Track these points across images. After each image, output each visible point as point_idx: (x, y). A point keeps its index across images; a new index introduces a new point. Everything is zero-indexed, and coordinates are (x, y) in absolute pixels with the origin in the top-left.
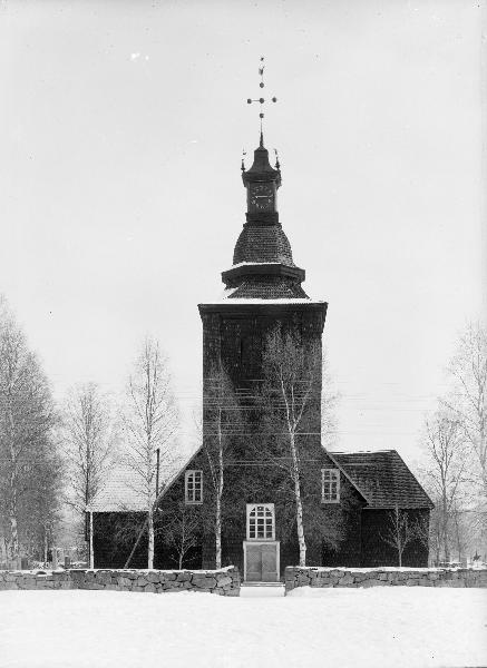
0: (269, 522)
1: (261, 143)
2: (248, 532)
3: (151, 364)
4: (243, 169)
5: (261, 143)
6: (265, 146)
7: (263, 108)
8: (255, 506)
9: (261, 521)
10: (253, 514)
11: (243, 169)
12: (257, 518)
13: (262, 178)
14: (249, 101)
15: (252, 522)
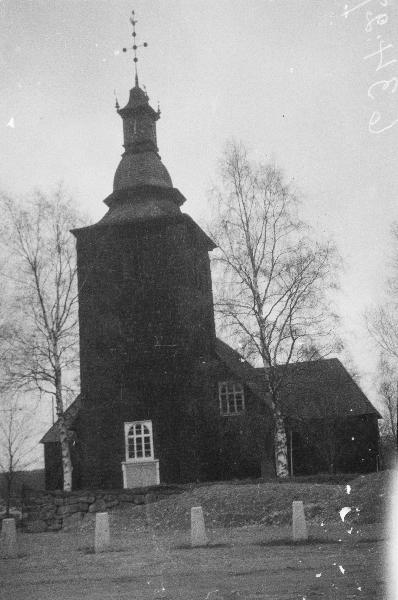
0: (147, 439)
1: (137, 83)
2: (151, 442)
3: (383, 313)
4: (117, 107)
5: (137, 83)
6: (141, 86)
7: (131, 41)
8: (133, 424)
9: (139, 440)
10: (131, 433)
11: (117, 107)
12: (135, 436)
13: (139, 115)
14: (145, 45)
15: (131, 441)
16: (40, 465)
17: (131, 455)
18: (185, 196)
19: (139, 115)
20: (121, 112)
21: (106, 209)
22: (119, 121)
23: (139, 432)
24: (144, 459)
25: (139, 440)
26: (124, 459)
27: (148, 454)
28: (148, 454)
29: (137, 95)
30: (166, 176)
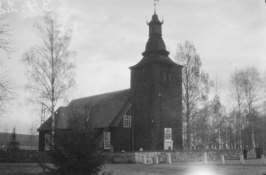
0: (129, 121)
4: (147, 22)
12: (126, 119)
13: (155, 25)
16: (168, 149)
17: (166, 139)
18: (169, 51)
19: (155, 25)
20: (148, 24)
21: (142, 57)
22: (148, 27)
23: (127, 119)
24: (169, 140)
25: (127, 121)
26: (165, 140)
27: (170, 139)
28: (170, 139)
29: (155, 17)
30: (164, 46)
